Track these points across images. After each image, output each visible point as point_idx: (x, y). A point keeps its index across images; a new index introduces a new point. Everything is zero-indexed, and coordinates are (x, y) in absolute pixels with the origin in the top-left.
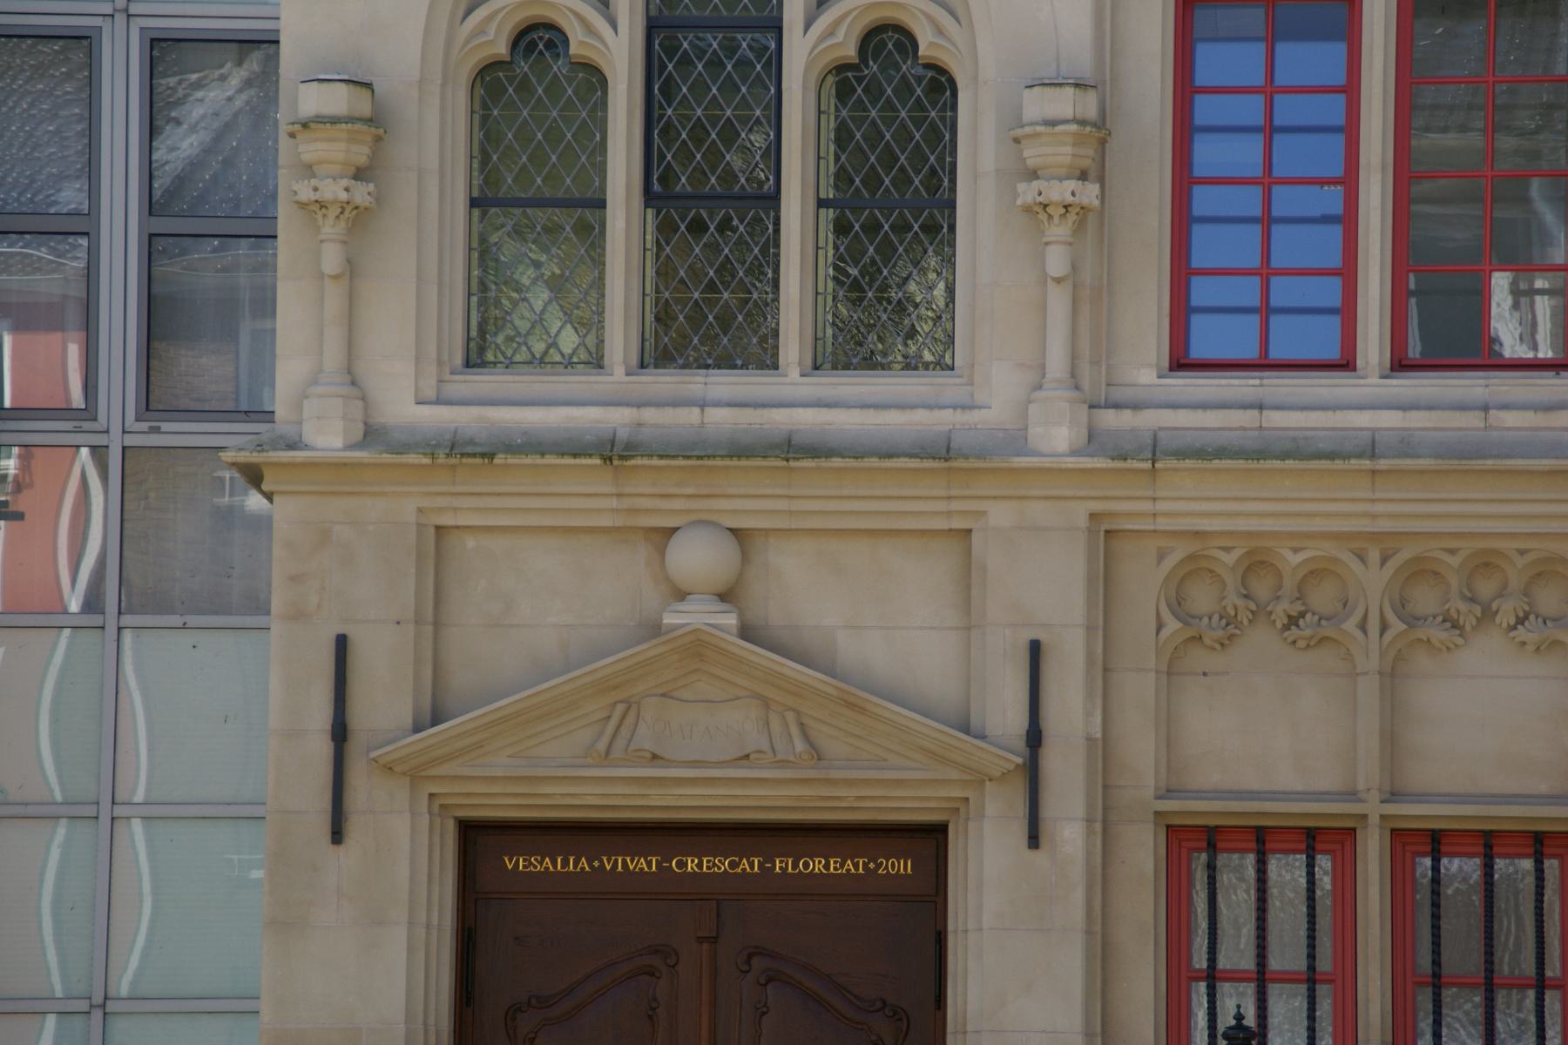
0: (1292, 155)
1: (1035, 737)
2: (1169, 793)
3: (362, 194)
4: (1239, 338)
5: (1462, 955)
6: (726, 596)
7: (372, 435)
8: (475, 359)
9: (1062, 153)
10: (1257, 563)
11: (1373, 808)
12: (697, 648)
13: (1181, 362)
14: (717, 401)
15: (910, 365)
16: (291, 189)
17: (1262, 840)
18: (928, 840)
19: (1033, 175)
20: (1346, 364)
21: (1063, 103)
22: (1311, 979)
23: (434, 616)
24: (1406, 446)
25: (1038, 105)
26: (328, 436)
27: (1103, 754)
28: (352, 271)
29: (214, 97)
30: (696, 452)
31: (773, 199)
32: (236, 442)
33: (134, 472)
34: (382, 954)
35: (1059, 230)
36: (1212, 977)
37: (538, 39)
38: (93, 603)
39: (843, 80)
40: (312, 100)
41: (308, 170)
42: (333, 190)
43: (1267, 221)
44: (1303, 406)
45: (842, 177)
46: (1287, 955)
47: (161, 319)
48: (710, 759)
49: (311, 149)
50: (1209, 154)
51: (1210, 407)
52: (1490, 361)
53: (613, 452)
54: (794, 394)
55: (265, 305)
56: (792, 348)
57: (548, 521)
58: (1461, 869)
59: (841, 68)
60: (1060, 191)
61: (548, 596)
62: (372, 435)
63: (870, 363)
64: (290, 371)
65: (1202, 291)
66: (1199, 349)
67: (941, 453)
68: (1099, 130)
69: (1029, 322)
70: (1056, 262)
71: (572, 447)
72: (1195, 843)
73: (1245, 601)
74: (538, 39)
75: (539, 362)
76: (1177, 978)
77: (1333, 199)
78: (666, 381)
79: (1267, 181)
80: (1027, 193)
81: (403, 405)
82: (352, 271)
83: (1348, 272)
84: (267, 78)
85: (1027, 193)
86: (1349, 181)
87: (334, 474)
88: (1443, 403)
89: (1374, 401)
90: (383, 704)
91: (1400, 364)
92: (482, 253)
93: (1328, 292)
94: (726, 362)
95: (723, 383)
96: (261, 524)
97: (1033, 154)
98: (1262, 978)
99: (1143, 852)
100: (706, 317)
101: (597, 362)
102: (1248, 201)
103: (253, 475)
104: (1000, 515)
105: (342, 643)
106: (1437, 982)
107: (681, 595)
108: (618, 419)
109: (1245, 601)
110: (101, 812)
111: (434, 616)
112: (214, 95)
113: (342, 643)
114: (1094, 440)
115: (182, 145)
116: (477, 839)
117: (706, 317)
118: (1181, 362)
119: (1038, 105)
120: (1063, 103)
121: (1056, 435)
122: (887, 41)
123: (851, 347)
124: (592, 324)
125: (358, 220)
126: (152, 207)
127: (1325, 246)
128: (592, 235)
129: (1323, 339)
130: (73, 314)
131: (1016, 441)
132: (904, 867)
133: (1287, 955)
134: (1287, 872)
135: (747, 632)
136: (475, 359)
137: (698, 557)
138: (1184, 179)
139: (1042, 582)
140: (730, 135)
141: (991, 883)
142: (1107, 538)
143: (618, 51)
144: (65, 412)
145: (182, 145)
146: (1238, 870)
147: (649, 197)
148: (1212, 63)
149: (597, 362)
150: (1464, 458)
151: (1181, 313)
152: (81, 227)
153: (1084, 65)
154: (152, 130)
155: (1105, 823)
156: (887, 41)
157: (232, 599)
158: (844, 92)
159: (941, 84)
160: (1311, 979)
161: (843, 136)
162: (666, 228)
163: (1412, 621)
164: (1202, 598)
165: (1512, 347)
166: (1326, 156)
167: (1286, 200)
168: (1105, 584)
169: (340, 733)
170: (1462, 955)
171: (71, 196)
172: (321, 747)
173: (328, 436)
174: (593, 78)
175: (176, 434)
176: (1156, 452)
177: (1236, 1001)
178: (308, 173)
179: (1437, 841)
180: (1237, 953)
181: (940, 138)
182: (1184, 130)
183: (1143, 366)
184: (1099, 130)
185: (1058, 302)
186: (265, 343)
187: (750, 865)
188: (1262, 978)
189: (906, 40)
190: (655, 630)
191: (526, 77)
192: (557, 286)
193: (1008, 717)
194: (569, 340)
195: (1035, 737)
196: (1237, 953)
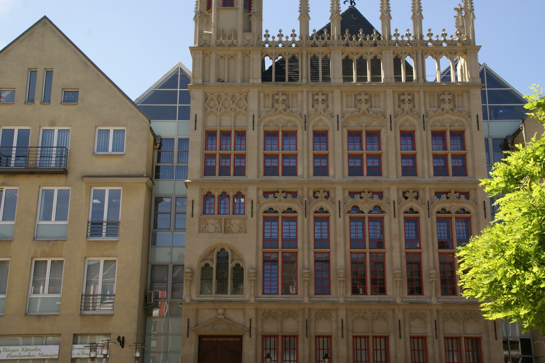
0: (273, 275)
1: (250, 327)
2: (262, 332)
3: (191, 279)
4: (268, 291)
5: (288, 347)
6: (223, 315)
7: (192, 300)
8: (201, 293)
9: (253, 275)
10: (270, 312)
11: (280, 334)
12: (220, 319)
13: (263, 294)
14: (222, 297)
15: (240, 294)
16: (185, 278)
17: (270, 336)
18: (241, 337)
19: (396, 278)
20: (278, 294)
21: (253, 271)
22: (275, 349)
23: (197, 316)
24: (283, 301)
25: (251, 271)
26: (188, 300)
27: (256, 329)
28: (190, 286)
29: (179, 270)
30: (221, 302)
31: (227, 279)
32: (179, 301)
33: (171, 304)
34: (191, 349)
35: (253, 282)
36: (266, 349)
37: (207, 265)
38: (167, 316)
39: (234, 269)
40: (187, 270)
41: (186, 277)
42: (189, 278)
43: (271, 281)
44: (274, 298)
45: (234, 277)
46: (272, 347)
47: (173, 290)
48: (221, 330)
49: (187, 275)
50: (266, 275)
51: (266, 298)
52: (290, 294)
53: (213, 302)
54: (229, 297)
55: (182, 288)
56: (229, 292)
57: (45, 138)
58: (287, 339)
59: (234, 268)
60: (253, 278)
61: (207, 315)
62: (192, 300)
63: (236, 294)
64: (184, 295)
65: (265, 287)
66: (265, 292)
67: (242, 302)
68: (256, 273)
69: (250, 291)
70: (252, 285)
71: (209, 301)
72: (264, 337)
73: (269, 315)
74: (207, 265)
75: (207, 294)
76: (263, 349)
77: (276, 279)
78: (218, 295)
79: (271, 277)
80: (250, 278)
81: (194, 297)
82: (190, 286)
83: (278, 286)
84: (183, 269)
85: (250, 278)
86: (278, 278)
87: (188, 304)
88: (286, 297)
89: (280, 297)
90: (192, 324)
91: (282, 294)
92: (202, 284)
93: (276, 287)
94: (223, 294)
95: (223, 295)
96: (182, 308)
97: (305, 275)
98: (270, 349)
99: (260, 338)
100: (221, 290)
101: (212, 293)
102: (269, 279)
103: (181, 304)
104: (247, 307)
105: (188, 319)
106: (285, 349)
107: (219, 315)
108: (214, 298)
109: (269, 315)
110: (167, 334)
111: (197, 316)
112: (178, 270)
113: (188, 319)
114: (256, 301)
115: (176, 274)
116: (200, 337)
117: (221, 290)
118: (263, 294)
119: (251, 271)
120: (253, 271)
121: (252, 300)
122: (238, 265)
123: (234, 292)
124: (211, 290)
125: (191, 281)
126: (173, 280)
127: (276, 283)
128: (211, 282)
129: (276, 292)
130: (106, 347)
131: (249, 301)
132: (238, 339)
133: (272, 347)
134: (272, 339)
135: (225, 318)
136: (201, 294)
137: (220, 311)
138: (264, 277)
139: (251, 313)
140: (224, 273)
141: (246, 340)
142: (257, 309)
143: (214, 266)
144: (165, 298)
145: (176, 274)
146: (268, 339)
147: (217, 279)
148: (266, 267)
149: (212, 293)
150: (288, 302)
151: (263, 289)
152: (166, 282)
153: (255, 267)
154: (173, 273)
155: (257, 335)
156: (238, 265)
157: (178, 315)
158: (234, 270)
159: (242, 269)
160: (275, 349)
161: (234, 273)
162: (218, 282)
163: (283, 317)
164: (265, 315)
165: (291, 292)
166: (276, 275)
167: (272, 279)
168: (257, 314)
169: (188, 327)
170: (288, 347)
171: (166, 279)
172: (187, 329)
173: (188, 300)
174: (212, 268)
175: (174, 300)
176: (261, 301)
177: (268, 351)
178: (186, 277)
179: (285, 336)
180: (268, 347)
181: (242, 274)
182: (264, 273)
183: (260, 294)
184: (256, 273)
185: (253, 288)
186: (182, 291)
187: (225, 339)
188: (270, 349)
189: (239, 265)
190: (217, 318)
191: (206, 269)
192: (208, 287)
193: (248, 325)
194: (209, 292)
195: (250, 327)
196: (268, 347)
